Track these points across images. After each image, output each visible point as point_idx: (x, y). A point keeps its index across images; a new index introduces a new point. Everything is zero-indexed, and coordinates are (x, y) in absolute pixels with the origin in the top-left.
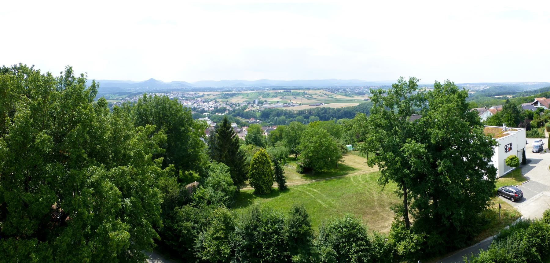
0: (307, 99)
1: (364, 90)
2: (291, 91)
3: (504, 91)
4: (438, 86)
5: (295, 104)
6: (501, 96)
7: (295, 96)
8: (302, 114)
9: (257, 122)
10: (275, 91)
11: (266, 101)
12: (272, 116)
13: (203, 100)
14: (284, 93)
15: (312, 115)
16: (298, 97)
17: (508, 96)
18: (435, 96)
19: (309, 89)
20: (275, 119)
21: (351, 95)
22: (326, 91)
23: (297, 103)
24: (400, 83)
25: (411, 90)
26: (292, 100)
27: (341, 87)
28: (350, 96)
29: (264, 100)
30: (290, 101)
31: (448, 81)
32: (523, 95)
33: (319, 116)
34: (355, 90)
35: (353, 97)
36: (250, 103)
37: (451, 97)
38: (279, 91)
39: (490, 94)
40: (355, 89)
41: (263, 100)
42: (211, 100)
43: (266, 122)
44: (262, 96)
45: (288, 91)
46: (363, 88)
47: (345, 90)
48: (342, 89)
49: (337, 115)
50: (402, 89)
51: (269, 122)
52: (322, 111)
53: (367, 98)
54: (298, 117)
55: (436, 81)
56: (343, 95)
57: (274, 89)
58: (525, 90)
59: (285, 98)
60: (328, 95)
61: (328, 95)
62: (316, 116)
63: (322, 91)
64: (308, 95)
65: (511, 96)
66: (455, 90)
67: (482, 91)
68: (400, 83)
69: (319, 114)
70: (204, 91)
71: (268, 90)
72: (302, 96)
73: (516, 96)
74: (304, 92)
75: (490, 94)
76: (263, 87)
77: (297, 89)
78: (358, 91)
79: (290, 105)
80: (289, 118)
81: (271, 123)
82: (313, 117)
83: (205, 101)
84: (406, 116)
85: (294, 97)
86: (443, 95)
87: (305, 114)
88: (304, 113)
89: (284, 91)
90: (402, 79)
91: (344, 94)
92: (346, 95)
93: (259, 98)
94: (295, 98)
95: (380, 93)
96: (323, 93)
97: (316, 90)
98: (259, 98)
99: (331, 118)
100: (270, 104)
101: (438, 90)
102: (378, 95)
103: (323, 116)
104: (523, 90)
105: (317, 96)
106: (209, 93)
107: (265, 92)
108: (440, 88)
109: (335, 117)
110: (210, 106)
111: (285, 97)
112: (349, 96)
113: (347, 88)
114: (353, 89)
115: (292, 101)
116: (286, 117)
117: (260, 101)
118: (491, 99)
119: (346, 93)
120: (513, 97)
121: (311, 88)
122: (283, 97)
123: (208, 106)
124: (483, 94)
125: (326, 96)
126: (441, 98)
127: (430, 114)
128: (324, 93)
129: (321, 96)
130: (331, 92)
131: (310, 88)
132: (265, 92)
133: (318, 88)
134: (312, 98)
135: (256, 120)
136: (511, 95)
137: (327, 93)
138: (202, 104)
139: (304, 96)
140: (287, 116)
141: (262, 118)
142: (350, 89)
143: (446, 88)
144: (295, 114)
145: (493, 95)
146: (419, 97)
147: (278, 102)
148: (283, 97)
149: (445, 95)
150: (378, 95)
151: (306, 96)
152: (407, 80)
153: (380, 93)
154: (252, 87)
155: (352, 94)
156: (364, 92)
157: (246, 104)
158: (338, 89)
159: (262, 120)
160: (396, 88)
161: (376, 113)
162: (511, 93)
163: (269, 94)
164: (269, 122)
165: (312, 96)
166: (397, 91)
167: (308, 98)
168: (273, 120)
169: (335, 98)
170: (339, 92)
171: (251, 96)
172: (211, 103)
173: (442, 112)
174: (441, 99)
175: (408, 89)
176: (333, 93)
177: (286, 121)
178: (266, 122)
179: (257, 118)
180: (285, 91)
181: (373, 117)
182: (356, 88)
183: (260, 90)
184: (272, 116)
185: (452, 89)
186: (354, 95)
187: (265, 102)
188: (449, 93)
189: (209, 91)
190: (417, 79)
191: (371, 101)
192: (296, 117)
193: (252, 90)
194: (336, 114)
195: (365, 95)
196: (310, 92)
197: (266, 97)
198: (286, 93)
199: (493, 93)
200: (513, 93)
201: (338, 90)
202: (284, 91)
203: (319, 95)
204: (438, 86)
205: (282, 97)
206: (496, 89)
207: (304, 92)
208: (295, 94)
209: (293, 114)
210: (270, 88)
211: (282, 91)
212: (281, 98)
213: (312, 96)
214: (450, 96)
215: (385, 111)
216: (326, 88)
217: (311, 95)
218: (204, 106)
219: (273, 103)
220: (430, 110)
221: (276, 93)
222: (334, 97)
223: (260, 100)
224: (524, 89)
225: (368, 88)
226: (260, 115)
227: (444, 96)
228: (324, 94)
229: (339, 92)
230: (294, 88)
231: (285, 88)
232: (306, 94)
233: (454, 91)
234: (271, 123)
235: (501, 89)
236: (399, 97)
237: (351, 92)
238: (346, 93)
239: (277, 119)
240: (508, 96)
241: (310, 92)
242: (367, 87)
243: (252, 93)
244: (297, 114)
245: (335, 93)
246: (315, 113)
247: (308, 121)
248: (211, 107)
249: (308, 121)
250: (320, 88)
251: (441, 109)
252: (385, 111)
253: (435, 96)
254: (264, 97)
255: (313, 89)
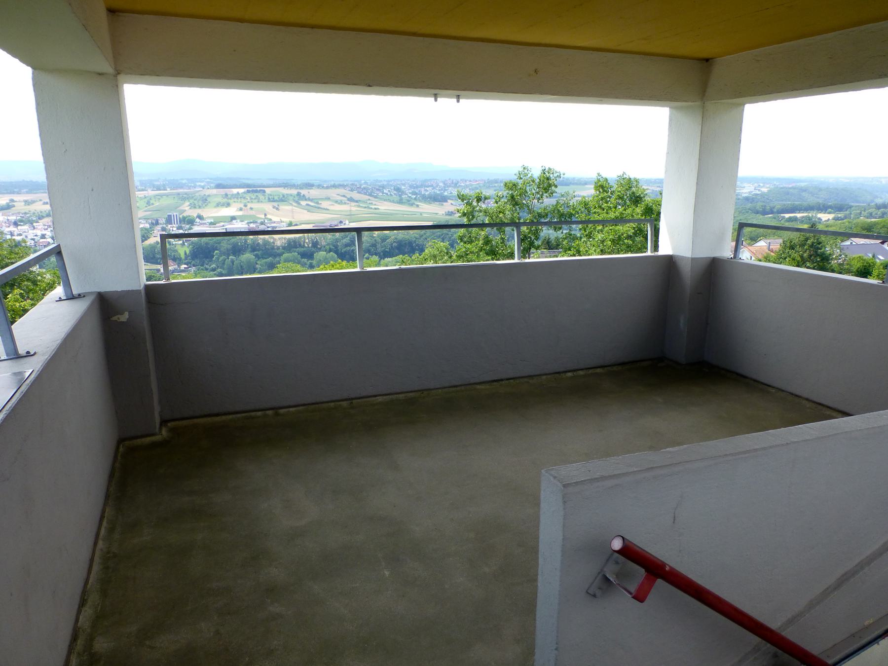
0: (306, 211)
1: (445, 190)
2: (264, 191)
3: (811, 200)
4: (602, 187)
5: (278, 222)
6: (799, 215)
7: (275, 204)
8: (296, 247)
9: (183, 271)
10: (222, 191)
11: (200, 217)
12: (222, 254)
13: (13, 218)
14: (248, 196)
15: (320, 249)
16: (284, 207)
17: (820, 215)
18: (595, 208)
19: (309, 186)
20: (228, 262)
21: (413, 201)
22: (352, 190)
23: (282, 222)
24: (521, 178)
25: (542, 195)
26: (270, 214)
27: (389, 181)
28: (412, 205)
29: (195, 216)
30: (263, 216)
31: (625, 176)
32: (871, 215)
33: (336, 252)
34: (423, 190)
35: (418, 206)
36: (157, 223)
37: (629, 211)
38: (235, 191)
39: (768, 208)
40: (422, 186)
41: (193, 213)
42: (40, 218)
43: (207, 269)
44: (187, 203)
45: (256, 191)
46: (441, 184)
47: (398, 190)
48: (392, 186)
49: (380, 250)
50: (524, 193)
51: (214, 270)
52: (345, 240)
53: (452, 209)
54: (286, 255)
55: (599, 174)
56: (393, 202)
57: (219, 186)
58: (879, 201)
59: (251, 209)
60: (357, 201)
61: (357, 201)
62: (330, 251)
63: (341, 191)
64: (309, 200)
65: (831, 216)
66: (639, 197)
67: (747, 199)
68: (521, 178)
69: (336, 246)
70: (13, 193)
71: (203, 187)
72: (294, 204)
73: (845, 217)
74: (299, 194)
75: (768, 208)
76: (188, 180)
77: (280, 186)
78: (429, 191)
79: (333, 235)
80: (264, 258)
81: (219, 270)
82: (323, 253)
83: (21, 221)
84: (530, 248)
85: (274, 207)
86: (610, 208)
87: (304, 246)
88: (300, 245)
89: (245, 190)
90: (526, 171)
91: (397, 198)
92: (401, 202)
93: (182, 208)
94: (277, 209)
95: (479, 199)
96: (344, 196)
97: (327, 188)
98: (182, 208)
99: (367, 255)
100: (211, 224)
101: (602, 195)
102: (475, 204)
103: (345, 252)
104: (872, 201)
105: (329, 203)
106: (29, 197)
107: (197, 194)
108: (607, 192)
109: (376, 254)
110: (39, 233)
111: (249, 205)
112: (410, 203)
113: (404, 185)
114: (417, 187)
115: (269, 216)
116: (256, 256)
117: (184, 218)
118: (768, 220)
119: (400, 196)
120: (836, 219)
121: (316, 183)
122: (245, 206)
123: (31, 234)
124: (749, 205)
125: (353, 204)
126: (607, 213)
127: (578, 245)
128: (349, 197)
129: (341, 203)
130: (365, 194)
131: (311, 182)
132: (197, 194)
133: (332, 183)
134: (319, 208)
135: (179, 266)
136: (829, 213)
137: (356, 195)
138: (12, 228)
139: (299, 204)
140: (259, 253)
141: (193, 259)
142: (411, 187)
143: (619, 192)
144: (278, 248)
145: (775, 210)
146: (559, 211)
147: (233, 218)
148: (245, 206)
149: (615, 208)
150: (475, 204)
151: (303, 203)
152: (536, 173)
153: (479, 199)
154: (157, 180)
155: (415, 199)
156: (446, 194)
157: (148, 226)
158: (383, 187)
159: (194, 266)
160: (511, 189)
161: (471, 242)
162: (830, 207)
163: (209, 199)
164: (214, 270)
165: (317, 203)
166: (512, 197)
167: (309, 209)
168: (224, 264)
169: (376, 209)
170: (383, 193)
171: (157, 204)
172: (40, 225)
173: (603, 242)
174: (605, 215)
175: (538, 193)
176: (370, 195)
177: (257, 266)
178: (207, 269)
179: (180, 259)
180: (248, 192)
181: (464, 249)
182: (424, 184)
183: (181, 188)
184: (222, 254)
185: (633, 193)
186: (420, 201)
187: (198, 220)
188: (625, 203)
189: (27, 193)
190: (556, 172)
191: (460, 217)
192: (280, 255)
193: (159, 189)
194: (378, 246)
195: (447, 201)
196: (314, 193)
197: (200, 207)
198: (253, 196)
199: (778, 205)
200: (839, 208)
201: (381, 188)
202: (245, 190)
203: (336, 202)
204: (602, 186)
205: (242, 206)
206: (788, 193)
207: (299, 194)
208: (276, 198)
209: (273, 248)
210: (208, 183)
211: (241, 191)
212: (241, 209)
213: (317, 203)
214: (625, 210)
215: (487, 237)
216: (352, 184)
217: (316, 200)
218: (20, 235)
219: (219, 222)
220: (581, 238)
221: (227, 195)
222: (373, 207)
223: (185, 214)
224: (876, 197)
225: (455, 184)
226: (188, 252)
227: (613, 209)
228: (349, 200)
229: (383, 193)
230: (271, 183)
231: (249, 182)
232: (304, 198)
233: (637, 200)
234: (219, 270)
235: (804, 194)
236: (518, 209)
237: (414, 193)
238: (400, 196)
239: (233, 262)
240: (820, 215)
241: (314, 193)
242: (452, 183)
243: (161, 196)
244: (284, 248)
245: (376, 197)
246: (328, 244)
247: (311, 264)
248: (43, 236)
249: (311, 264)
250: (337, 183)
251: (600, 236)
252: (487, 237)
253: (595, 208)
254: (195, 207)
255: (319, 186)
